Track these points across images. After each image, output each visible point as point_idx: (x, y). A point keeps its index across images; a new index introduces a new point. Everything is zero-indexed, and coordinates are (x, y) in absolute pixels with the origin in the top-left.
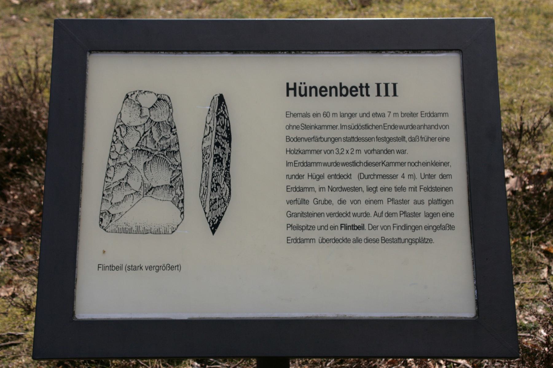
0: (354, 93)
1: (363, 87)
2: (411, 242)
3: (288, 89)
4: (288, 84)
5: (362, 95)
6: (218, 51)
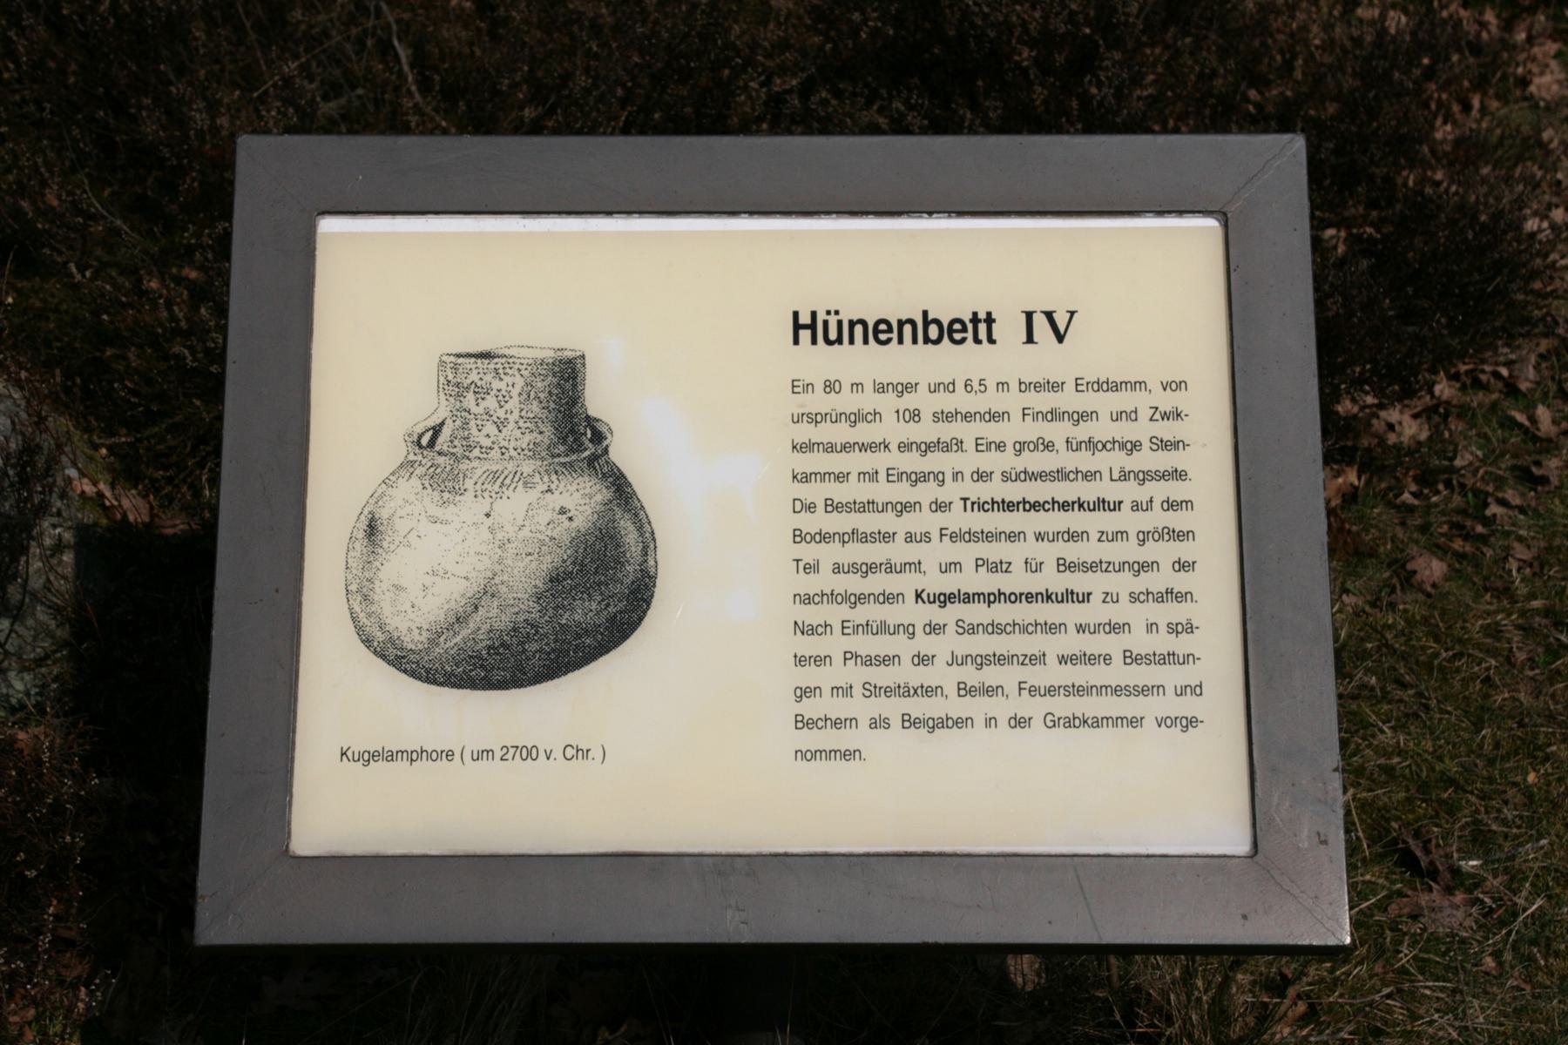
0: (957, 336)
1: (980, 321)
2: (982, 664)
3: (797, 327)
4: (796, 314)
5: (977, 341)
6: (745, 213)
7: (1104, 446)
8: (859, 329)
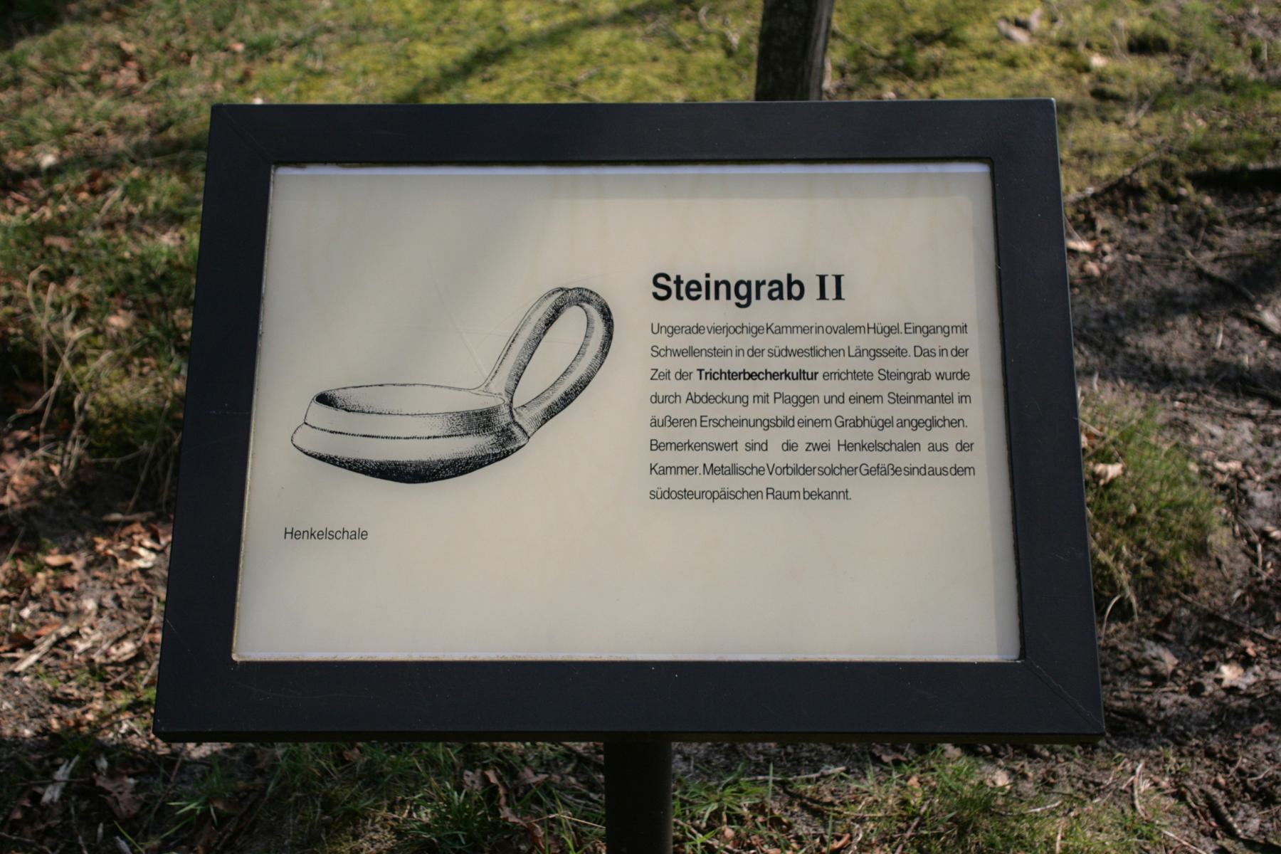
7: (735, 330)
8: (723, 288)
